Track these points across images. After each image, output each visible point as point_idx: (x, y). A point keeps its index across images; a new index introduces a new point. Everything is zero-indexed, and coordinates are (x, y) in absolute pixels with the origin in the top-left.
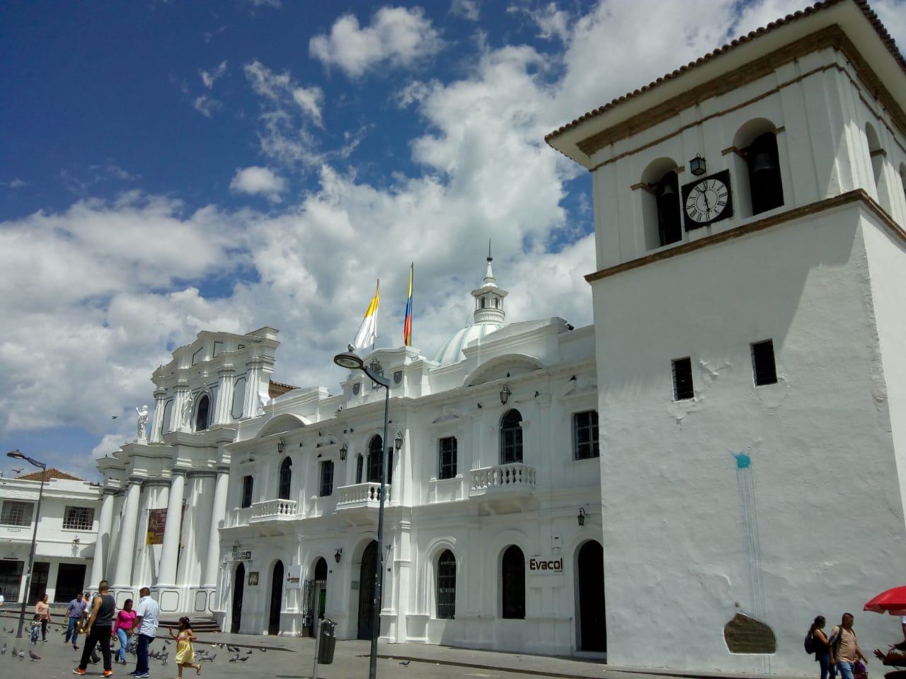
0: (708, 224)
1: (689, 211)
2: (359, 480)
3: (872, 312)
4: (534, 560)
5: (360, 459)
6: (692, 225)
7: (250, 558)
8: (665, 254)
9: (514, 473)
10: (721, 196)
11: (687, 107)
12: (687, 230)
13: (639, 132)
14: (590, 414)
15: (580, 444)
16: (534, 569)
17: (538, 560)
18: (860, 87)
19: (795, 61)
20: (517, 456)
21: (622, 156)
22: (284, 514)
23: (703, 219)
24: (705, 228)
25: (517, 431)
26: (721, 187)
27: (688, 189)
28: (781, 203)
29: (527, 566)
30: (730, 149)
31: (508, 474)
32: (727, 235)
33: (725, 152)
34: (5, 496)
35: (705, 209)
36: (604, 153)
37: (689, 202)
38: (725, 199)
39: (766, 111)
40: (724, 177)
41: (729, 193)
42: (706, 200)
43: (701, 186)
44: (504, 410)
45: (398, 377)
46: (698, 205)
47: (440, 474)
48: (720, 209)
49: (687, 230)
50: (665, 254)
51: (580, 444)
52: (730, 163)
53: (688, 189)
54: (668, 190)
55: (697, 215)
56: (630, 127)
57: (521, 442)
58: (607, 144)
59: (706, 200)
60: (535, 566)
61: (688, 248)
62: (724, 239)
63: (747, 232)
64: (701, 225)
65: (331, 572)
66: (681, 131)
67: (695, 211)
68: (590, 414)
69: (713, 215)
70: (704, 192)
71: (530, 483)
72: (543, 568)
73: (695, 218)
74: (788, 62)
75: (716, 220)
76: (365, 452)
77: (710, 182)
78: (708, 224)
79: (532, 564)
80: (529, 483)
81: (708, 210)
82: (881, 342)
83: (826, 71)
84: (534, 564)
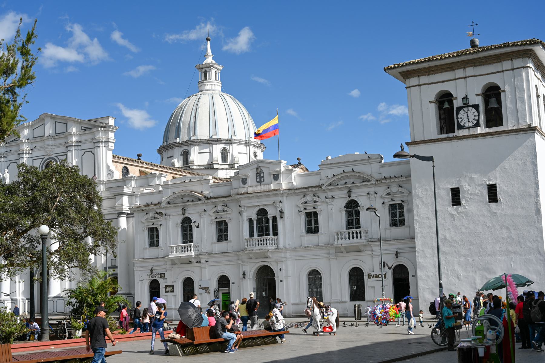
0: (469, 128)
1: (460, 120)
2: (251, 235)
3: (538, 178)
4: (370, 274)
5: (251, 221)
6: (461, 127)
7: (164, 277)
8: (448, 139)
9: (266, 240)
10: (475, 116)
11: (459, 68)
12: (458, 129)
13: (433, 74)
14: (223, 222)
15: (308, 226)
16: (371, 278)
17: (372, 274)
18: (542, 81)
19: (512, 60)
20: (260, 234)
21: (425, 84)
22: (186, 252)
23: (466, 125)
24: (467, 129)
25: (189, 226)
26: (475, 112)
27: (459, 109)
28: (501, 124)
29: (366, 277)
30: (480, 94)
31: (261, 240)
32: (478, 136)
33: (477, 95)
34: (416, 202)
35: (467, 120)
36: (414, 81)
37: (460, 116)
38: (477, 118)
39: (495, 79)
40: (476, 107)
41: (479, 116)
42: (468, 117)
43: (465, 109)
44: (183, 217)
45: (276, 177)
46: (463, 117)
47: (217, 239)
48: (475, 122)
49: (458, 129)
50: (448, 139)
51: (308, 226)
52: (479, 101)
53: (459, 109)
54: (446, 106)
55: (463, 123)
56: (429, 71)
57: (359, 216)
58: (416, 76)
59: (468, 117)
60: (371, 277)
61: (460, 138)
62: (476, 137)
63: (487, 135)
64: (466, 128)
65: (233, 283)
66: (456, 79)
67: (462, 121)
68: (223, 222)
69: (471, 124)
70: (467, 112)
71: (274, 244)
72: (375, 278)
73: (462, 124)
74: (508, 60)
75: (472, 127)
76: (254, 218)
77: (470, 108)
78: (469, 128)
79: (369, 276)
80: (271, 245)
81: (469, 121)
82: (540, 190)
83: (525, 69)
84: (370, 276)
